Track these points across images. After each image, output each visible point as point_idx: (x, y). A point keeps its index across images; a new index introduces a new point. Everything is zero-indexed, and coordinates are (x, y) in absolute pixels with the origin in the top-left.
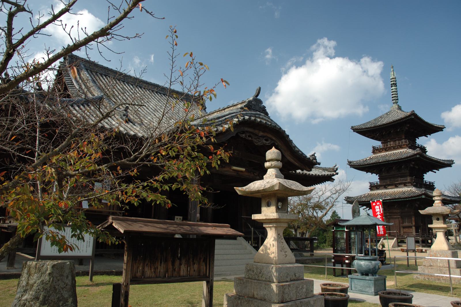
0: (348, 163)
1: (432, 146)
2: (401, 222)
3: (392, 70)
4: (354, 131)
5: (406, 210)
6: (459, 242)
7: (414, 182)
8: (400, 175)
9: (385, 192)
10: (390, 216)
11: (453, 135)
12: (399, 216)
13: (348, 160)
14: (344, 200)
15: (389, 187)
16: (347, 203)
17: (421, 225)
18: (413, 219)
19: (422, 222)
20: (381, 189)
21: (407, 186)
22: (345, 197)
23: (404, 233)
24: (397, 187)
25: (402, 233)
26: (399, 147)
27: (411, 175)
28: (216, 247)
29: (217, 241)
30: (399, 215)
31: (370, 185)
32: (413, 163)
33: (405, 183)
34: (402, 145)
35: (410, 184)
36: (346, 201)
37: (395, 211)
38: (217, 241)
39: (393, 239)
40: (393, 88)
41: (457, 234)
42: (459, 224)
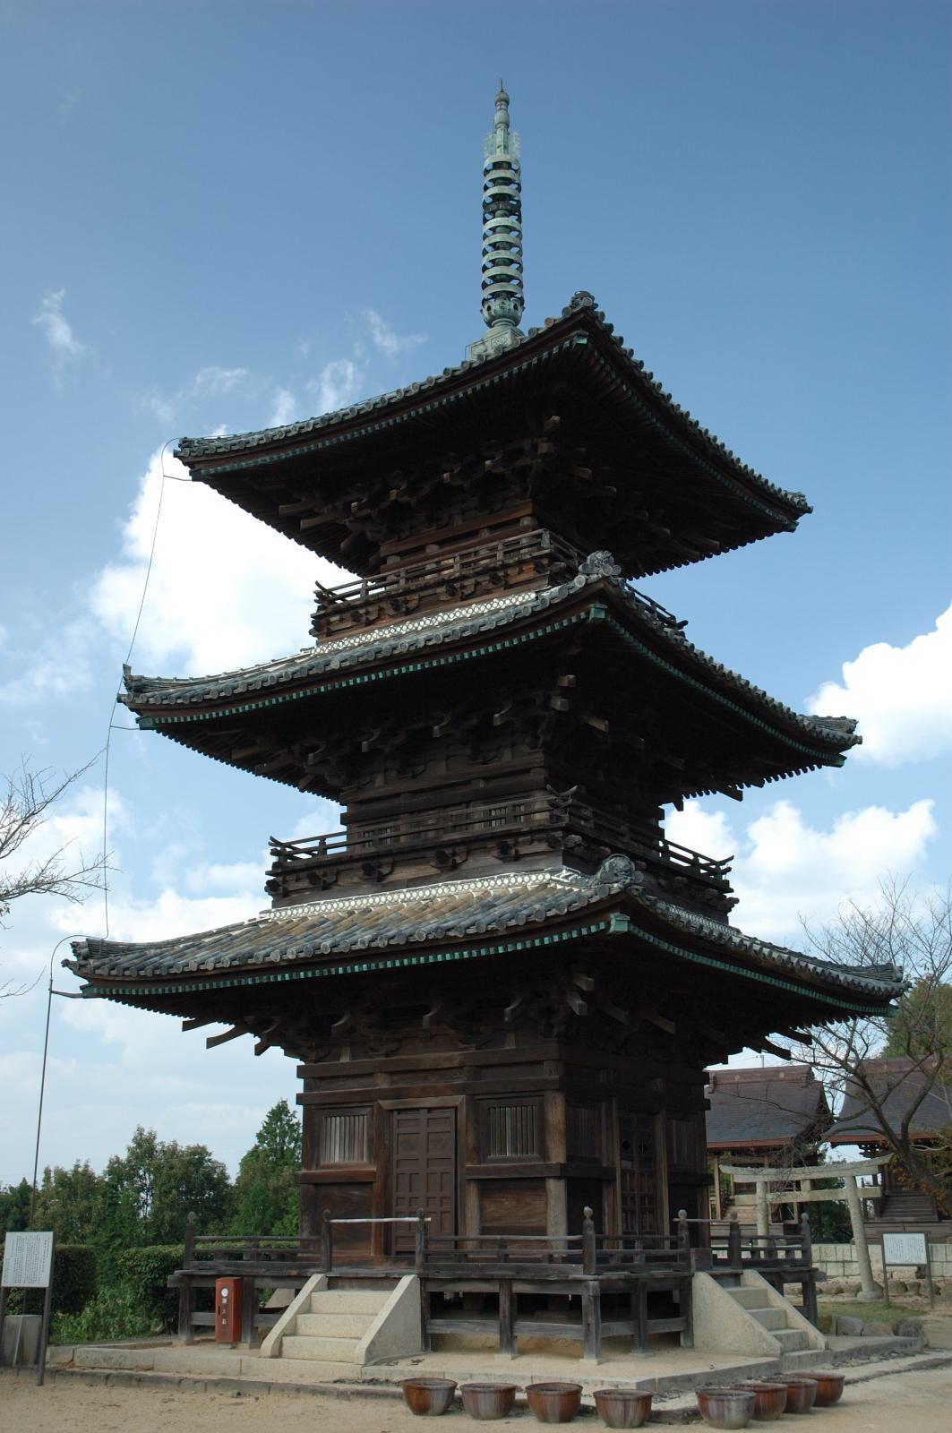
0: (124, 691)
1: (715, 606)
2: (471, 1141)
3: (498, 116)
4: (196, 476)
5: (510, 1045)
6: (879, 1280)
7: (568, 830)
8: (482, 784)
9: (367, 910)
10: (398, 1094)
11: (892, 791)
12: (459, 1099)
13: (126, 668)
14: (66, 963)
15: (402, 874)
16: (87, 993)
17: (619, 1164)
18: (556, 1113)
19: (625, 1146)
20: (346, 893)
21: (518, 858)
22: (75, 946)
23: (484, 1230)
24: (455, 867)
25: (472, 1228)
26: (485, 579)
27: (557, 780)
28: (876, 1246)
29: (880, 1246)
30: (461, 1089)
31: (275, 859)
32: (567, 679)
33: (509, 834)
34: (505, 566)
35: (543, 847)
36: (78, 969)
37: (429, 1057)
38: (880, 1246)
39: (389, 1282)
40: (492, 223)
41: (871, 1231)
42: (881, 1168)
